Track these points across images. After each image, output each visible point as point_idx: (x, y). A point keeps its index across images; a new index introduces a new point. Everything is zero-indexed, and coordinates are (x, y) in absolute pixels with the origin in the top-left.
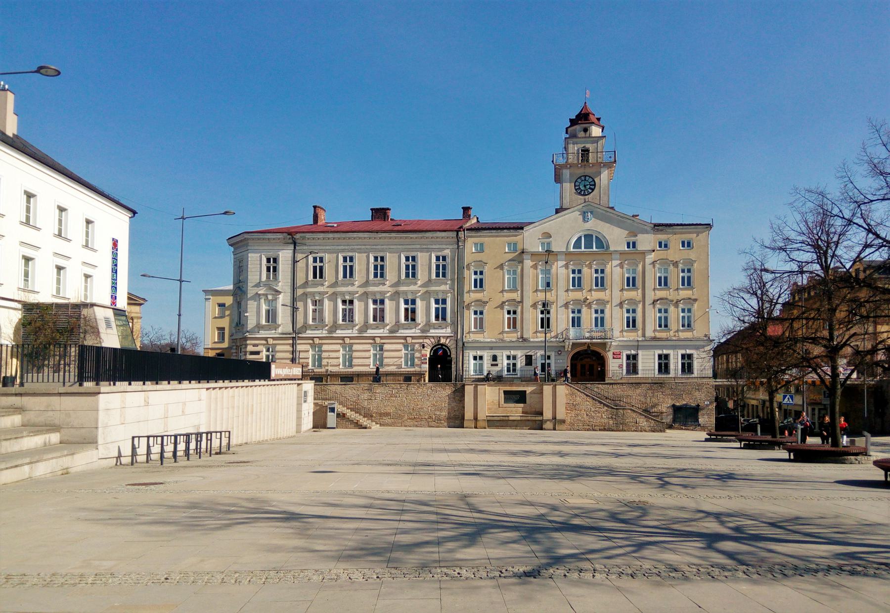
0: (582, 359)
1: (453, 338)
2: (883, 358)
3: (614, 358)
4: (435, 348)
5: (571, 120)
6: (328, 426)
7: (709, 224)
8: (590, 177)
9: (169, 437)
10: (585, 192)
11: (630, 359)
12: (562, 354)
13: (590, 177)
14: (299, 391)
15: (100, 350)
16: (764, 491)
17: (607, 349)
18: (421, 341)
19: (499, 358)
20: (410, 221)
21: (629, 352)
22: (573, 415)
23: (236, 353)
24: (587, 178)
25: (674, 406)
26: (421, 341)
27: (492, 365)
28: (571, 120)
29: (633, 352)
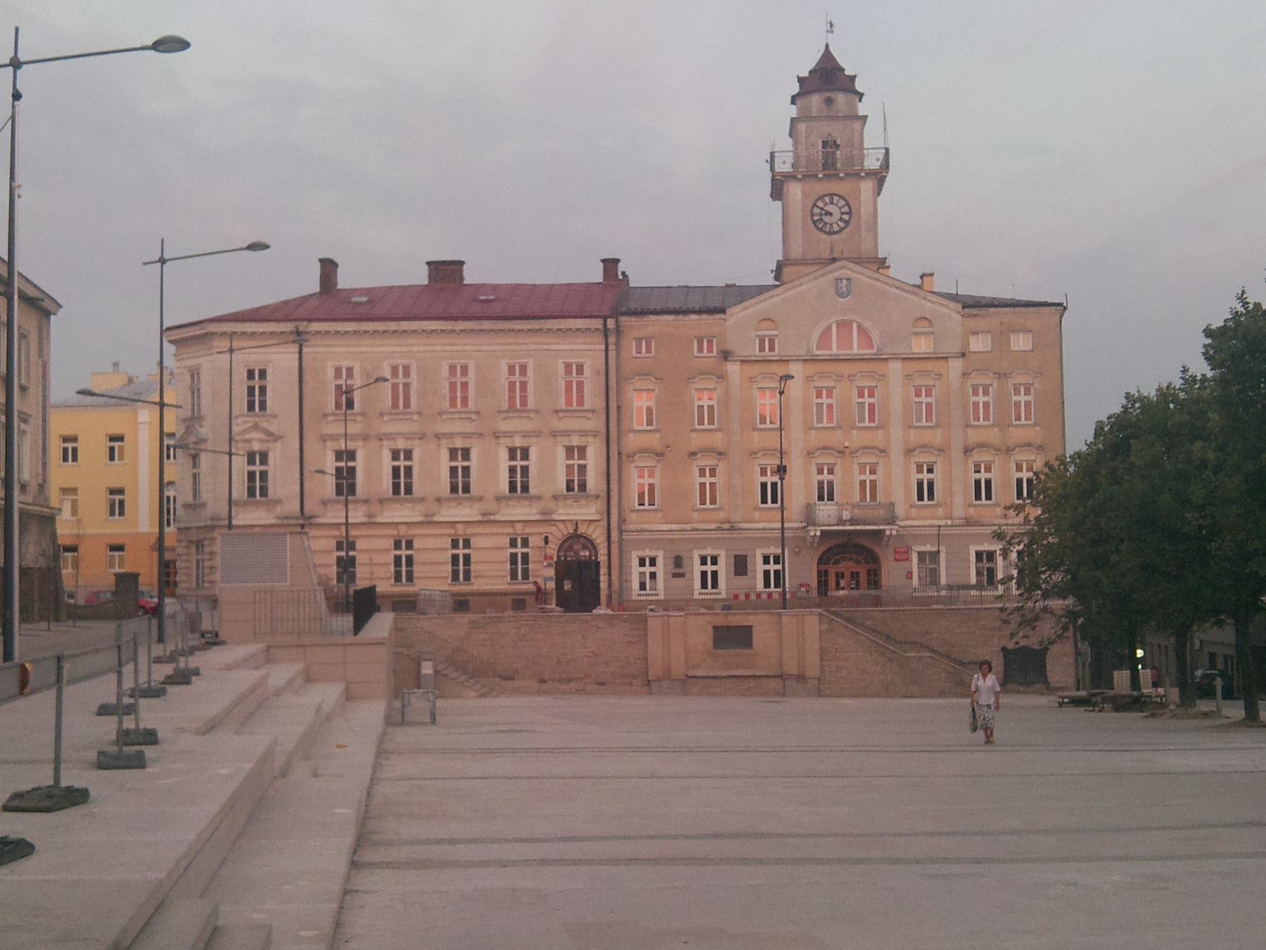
0: (837, 562)
1: (601, 523)
2: (566, 588)
3: (896, 560)
4: (566, 545)
5: (801, 80)
6: (16, 103)
7: (1061, 304)
8: (841, 197)
9: (263, 631)
10: (845, 213)
11: (982, 561)
12: (802, 553)
13: (841, 197)
14: (340, 435)
15: (1161, 687)
16: (947, 746)
17: (884, 544)
18: (542, 529)
19: (685, 563)
20: (495, 288)
21: (980, 548)
22: (834, 669)
23: (188, 555)
24: (836, 199)
25: (1003, 649)
26: (542, 529)
27: (675, 575)
28: (801, 80)
29: (929, 548)
